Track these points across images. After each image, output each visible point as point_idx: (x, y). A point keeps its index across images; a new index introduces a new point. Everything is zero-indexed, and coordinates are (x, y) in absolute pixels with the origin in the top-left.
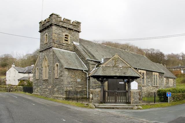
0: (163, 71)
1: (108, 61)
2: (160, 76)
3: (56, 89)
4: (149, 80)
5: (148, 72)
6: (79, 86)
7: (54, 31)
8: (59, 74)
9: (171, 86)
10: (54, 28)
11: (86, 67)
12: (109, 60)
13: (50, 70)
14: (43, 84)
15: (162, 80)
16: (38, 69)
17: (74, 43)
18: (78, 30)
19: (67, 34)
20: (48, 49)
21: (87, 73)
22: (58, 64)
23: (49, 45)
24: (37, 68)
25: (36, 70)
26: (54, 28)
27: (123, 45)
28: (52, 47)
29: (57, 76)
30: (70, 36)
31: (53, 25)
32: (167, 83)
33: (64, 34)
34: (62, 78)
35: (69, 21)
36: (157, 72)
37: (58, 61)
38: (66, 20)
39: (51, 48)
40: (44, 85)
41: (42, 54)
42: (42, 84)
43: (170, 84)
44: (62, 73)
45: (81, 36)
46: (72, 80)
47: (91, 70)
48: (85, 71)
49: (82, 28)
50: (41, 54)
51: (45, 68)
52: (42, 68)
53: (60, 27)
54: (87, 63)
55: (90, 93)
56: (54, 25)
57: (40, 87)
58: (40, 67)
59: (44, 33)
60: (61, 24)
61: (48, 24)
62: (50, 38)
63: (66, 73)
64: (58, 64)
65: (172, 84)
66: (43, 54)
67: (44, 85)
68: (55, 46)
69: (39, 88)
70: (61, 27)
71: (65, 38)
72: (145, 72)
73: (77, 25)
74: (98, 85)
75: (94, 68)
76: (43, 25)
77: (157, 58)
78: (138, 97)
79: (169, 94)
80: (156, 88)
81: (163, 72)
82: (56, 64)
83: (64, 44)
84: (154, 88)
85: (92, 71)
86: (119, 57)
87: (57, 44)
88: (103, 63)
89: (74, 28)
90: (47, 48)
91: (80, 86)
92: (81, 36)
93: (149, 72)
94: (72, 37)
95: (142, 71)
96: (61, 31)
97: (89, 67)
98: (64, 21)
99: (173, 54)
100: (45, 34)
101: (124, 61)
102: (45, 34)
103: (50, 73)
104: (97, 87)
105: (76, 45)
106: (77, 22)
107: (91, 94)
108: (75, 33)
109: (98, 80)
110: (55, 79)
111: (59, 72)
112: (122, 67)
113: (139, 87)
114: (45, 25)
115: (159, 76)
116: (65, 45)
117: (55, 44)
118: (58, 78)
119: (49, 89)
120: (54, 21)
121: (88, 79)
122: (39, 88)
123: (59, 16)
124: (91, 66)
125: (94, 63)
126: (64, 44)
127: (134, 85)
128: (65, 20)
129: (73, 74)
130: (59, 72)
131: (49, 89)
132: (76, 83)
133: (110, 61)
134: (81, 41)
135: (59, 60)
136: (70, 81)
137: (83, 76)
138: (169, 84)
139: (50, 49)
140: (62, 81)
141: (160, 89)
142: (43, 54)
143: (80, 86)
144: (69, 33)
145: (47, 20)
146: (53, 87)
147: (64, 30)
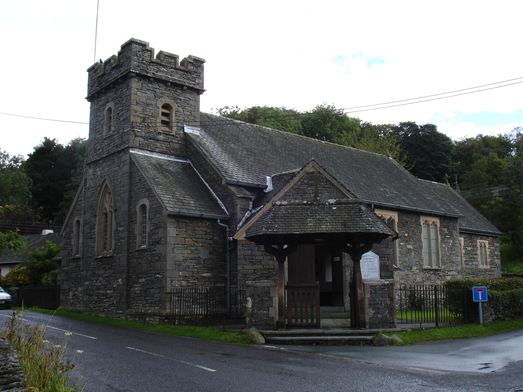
0: (456, 212)
1: (288, 185)
2: (446, 230)
3: (137, 289)
4: (410, 247)
5: (405, 218)
6: (205, 275)
7: (133, 97)
8: (150, 236)
9: (485, 267)
10: (135, 84)
11: (223, 207)
12: (292, 183)
13: (122, 224)
14: (97, 272)
15: (454, 245)
16: (78, 222)
17: (188, 130)
18: (195, 87)
19: (168, 101)
20: (113, 154)
21: (228, 230)
22: (146, 201)
23: (118, 142)
24: (76, 219)
25: (72, 227)
26: (135, 84)
27: (315, 113)
28: (129, 148)
29: (144, 243)
30: (174, 106)
31: (131, 77)
32: (471, 256)
33: (160, 105)
34: (159, 249)
35: (173, 61)
36: (435, 216)
37: (147, 194)
38: (165, 55)
39: (123, 150)
40: (99, 276)
41: (95, 171)
42: (95, 273)
43: (479, 259)
44: (161, 232)
45: (210, 104)
46: (186, 255)
47: (239, 215)
48: (222, 221)
49: (210, 77)
50: (91, 171)
51: (103, 217)
52: (93, 219)
53: (151, 82)
54: (227, 197)
55: (248, 294)
56: (135, 75)
57: (87, 283)
58: (88, 216)
59: (104, 102)
60: (151, 71)
61: (116, 75)
62: (121, 119)
63: (172, 231)
64: (146, 201)
65: (488, 260)
66: (99, 173)
67: (99, 276)
68: (138, 144)
69: (80, 289)
70: (152, 79)
71: (163, 114)
72: (395, 216)
73: (195, 69)
74: (261, 267)
75: (248, 210)
76: (98, 78)
77: (421, 149)
78: (386, 304)
79: (480, 292)
80: (433, 277)
81: (453, 215)
82: (141, 202)
83: (160, 134)
84: (428, 275)
85: (241, 220)
86: (321, 171)
87: (142, 137)
88: (274, 193)
89: (187, 76)
90: (112, 152)
91: (209, 274)
92: (210, 104)
93: (410, 215)
94: (180, 109)
95: (387, 215)
96: (152, 95)
97: (234, 209)
98: (159, 61)
99: (481, 136)
100: (107, 108)
101: (334, 182)
102: (104, 105)
103: (120, 234)
104: (259, 273)
105: (193, 135)
106: (195, 60)
107: (249, 299)
108: (188, 96)
109: (270, 251)
110: (137, 254)
111: (148, 230)
112: (336, 204)
113: (386, 270)
114: (106, 77)
115: (441, 230)
116: (161, 137)
117: (136, 136)
118: (145, 250)
119: (114, 289)
120: (134, 66)
121: (229, 249)
122: (80, 289)
123: (148, 48)
124: (240, 204)
125: (248, 194)
126: (160, 134)
127: (370, 265)
128: (162, 58)
129: (190, 232)
130: (148, 230)
131: (114, 289)
132: (198, 264)
133: (296, 184)
134: (207, 122)
135: (149, 190)
136: (181, 259)
137: (215, 238)
138: (480, 259)
139: (122, 154)
140: (159, 260)
141: (449, 278)
142: (99, 173)
143: (209, 274)
144: (175, 99)
145: (112, 61)
146: (129, 283)
147: (160, 89)
